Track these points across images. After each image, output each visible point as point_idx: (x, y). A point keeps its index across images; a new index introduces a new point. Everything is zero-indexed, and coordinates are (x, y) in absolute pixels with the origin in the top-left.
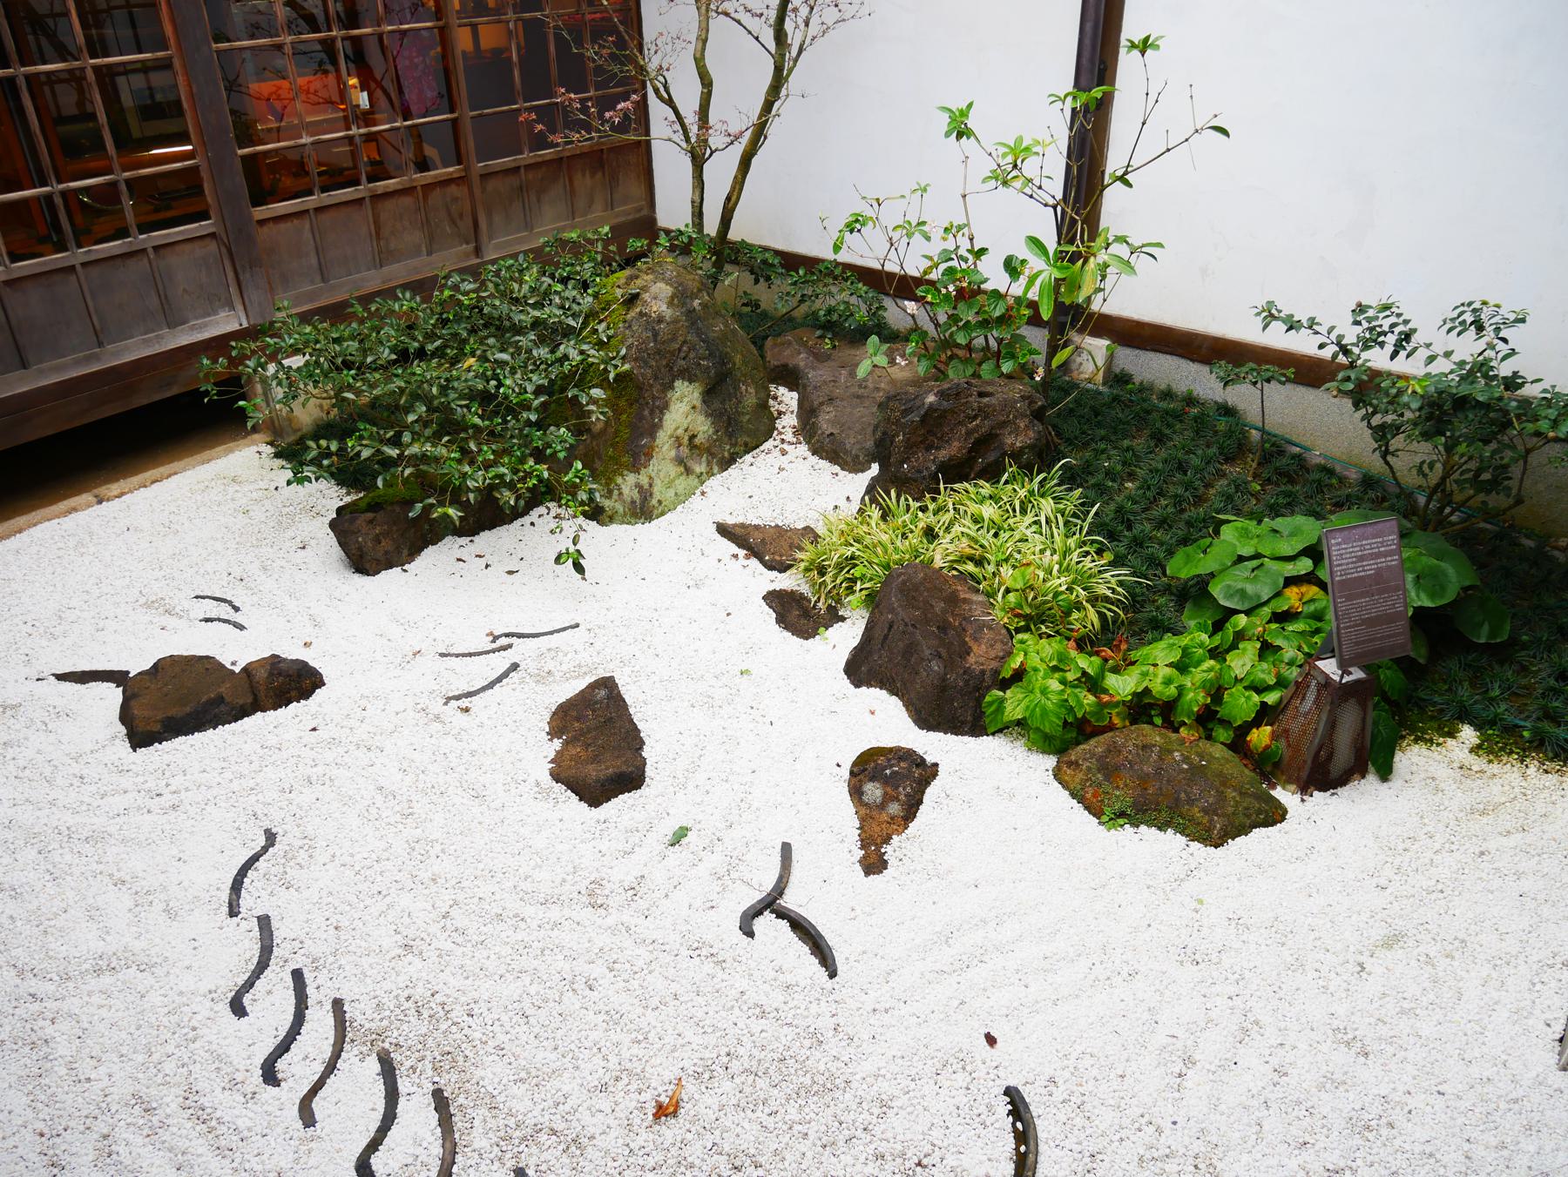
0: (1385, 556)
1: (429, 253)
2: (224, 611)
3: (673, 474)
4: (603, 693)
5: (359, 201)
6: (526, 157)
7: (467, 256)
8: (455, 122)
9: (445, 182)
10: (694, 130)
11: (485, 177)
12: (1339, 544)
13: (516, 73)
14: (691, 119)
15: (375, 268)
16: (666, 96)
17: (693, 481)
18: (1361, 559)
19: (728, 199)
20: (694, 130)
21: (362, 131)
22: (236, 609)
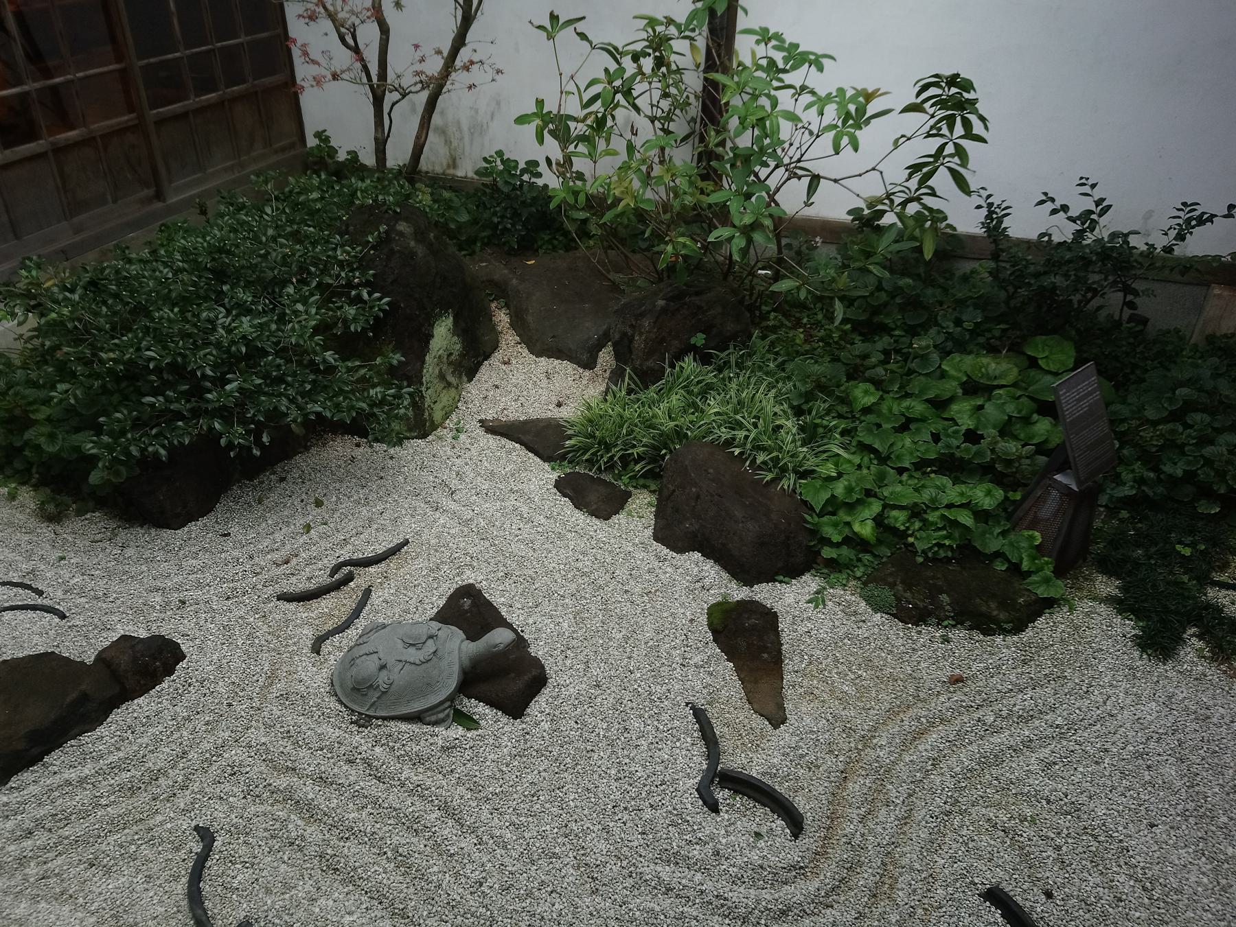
0: (1091, 394)
1: (115, 202)
2: (29, 598)
3: (440, 389)
4: (467, 602)
5: (41, 156)
6: (192, 102)
7: (150, 200)
8: (123, 72)
9: (121, 131)
10: (375, 79)
11: (161, 122)
12: (1065, 393)
13: (175, 21)
14: (374, 69)
15: (66, 220)
16: (351, 42)
17: (453, 392)
18: (1079, 400)
19: (418, 137)
20: (375, 79)
21: (37, 85)
22: (40, 593)
